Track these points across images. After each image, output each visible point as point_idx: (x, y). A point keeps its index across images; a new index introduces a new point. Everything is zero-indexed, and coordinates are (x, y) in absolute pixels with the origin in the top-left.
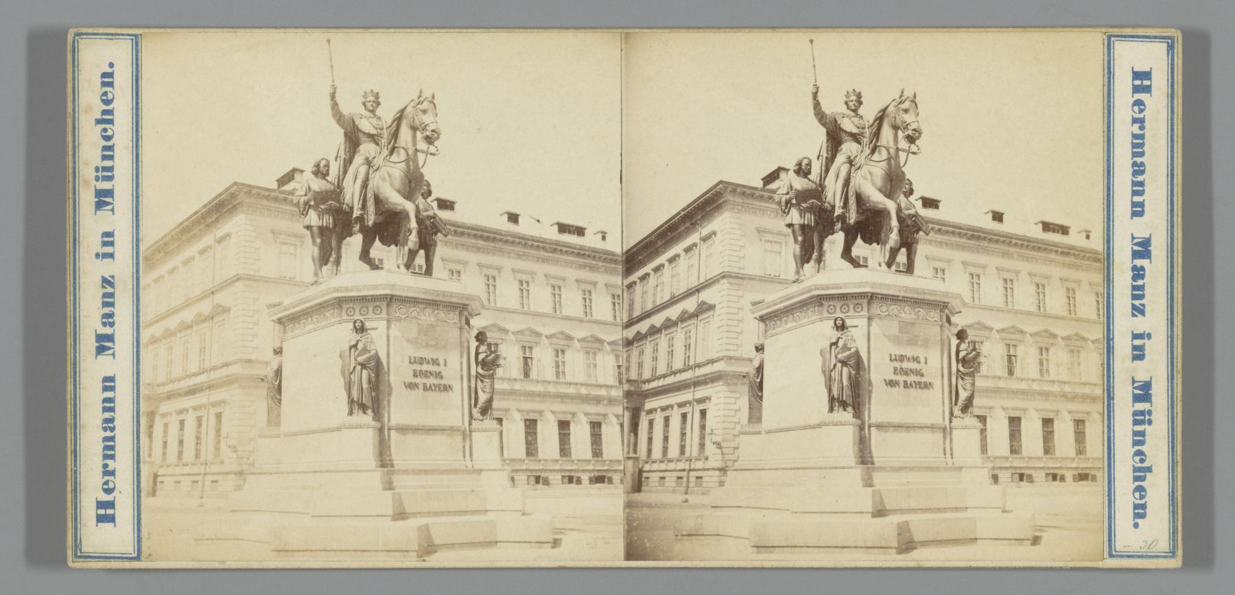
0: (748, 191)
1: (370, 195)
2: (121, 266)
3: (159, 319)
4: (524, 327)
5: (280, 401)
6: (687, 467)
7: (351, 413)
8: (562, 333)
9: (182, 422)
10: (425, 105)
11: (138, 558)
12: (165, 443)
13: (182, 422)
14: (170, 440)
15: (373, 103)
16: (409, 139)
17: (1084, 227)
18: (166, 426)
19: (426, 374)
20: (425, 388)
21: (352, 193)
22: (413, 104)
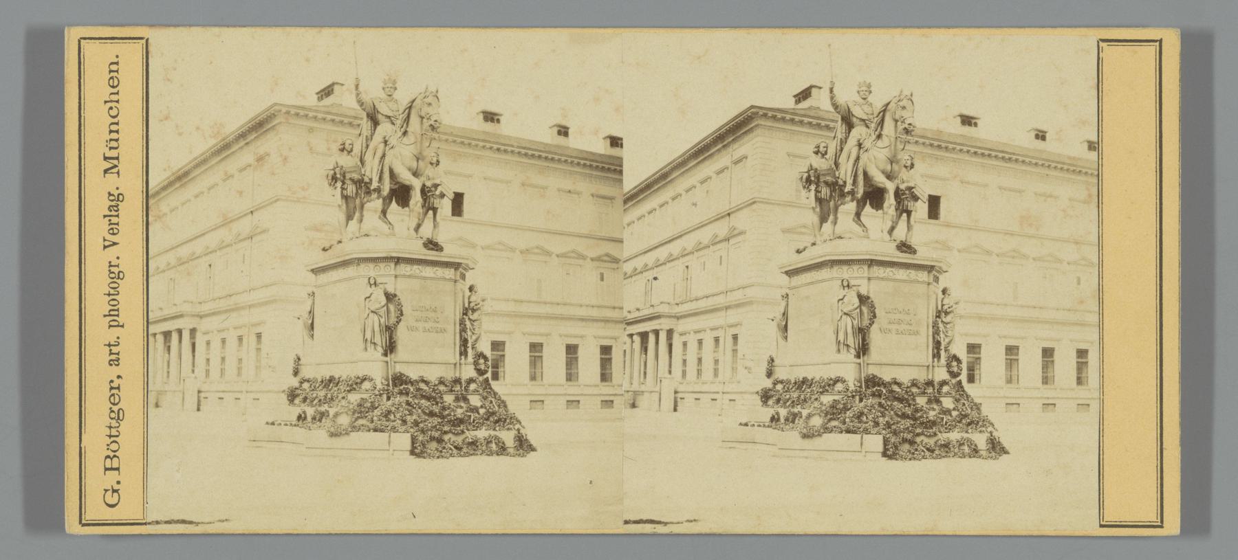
0: (302, 113)
1: (860, 173)
2: (129, 183)
3: (832, 279)
4: (603, 253)
5: (786, 338)
6: (720, 390)
7: (839, 351)
8: (607, 255)
9: (700, 342)
10: (904, 103)
11: (1161, 527)
12: (700, 360)
13: (700, 342)
14: (688, 358)
15: (391, 88)
16: (892, 128)
17: (1069, 143)
18: (685, 344)
19: (900, 322)
20: (621, 308)
21: (845, 172)
22: (895, 100)
